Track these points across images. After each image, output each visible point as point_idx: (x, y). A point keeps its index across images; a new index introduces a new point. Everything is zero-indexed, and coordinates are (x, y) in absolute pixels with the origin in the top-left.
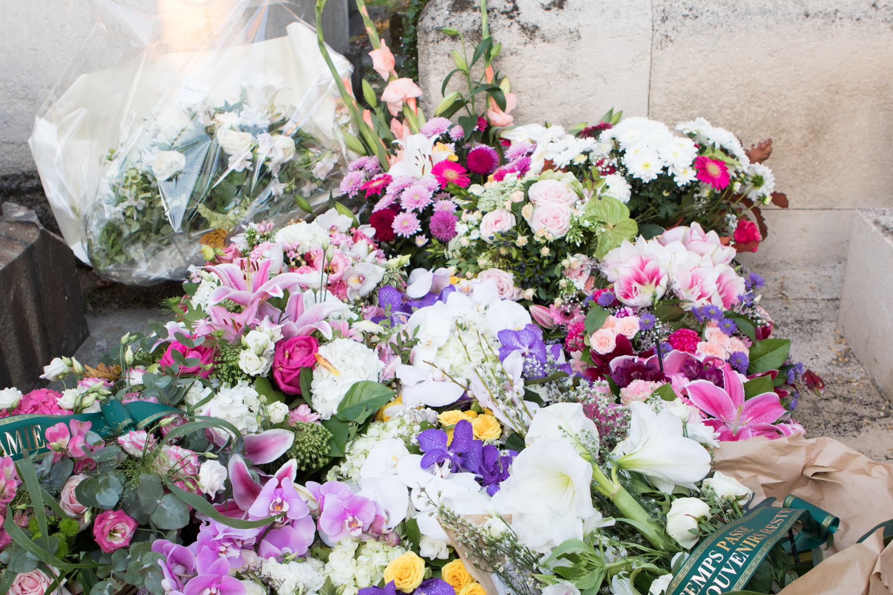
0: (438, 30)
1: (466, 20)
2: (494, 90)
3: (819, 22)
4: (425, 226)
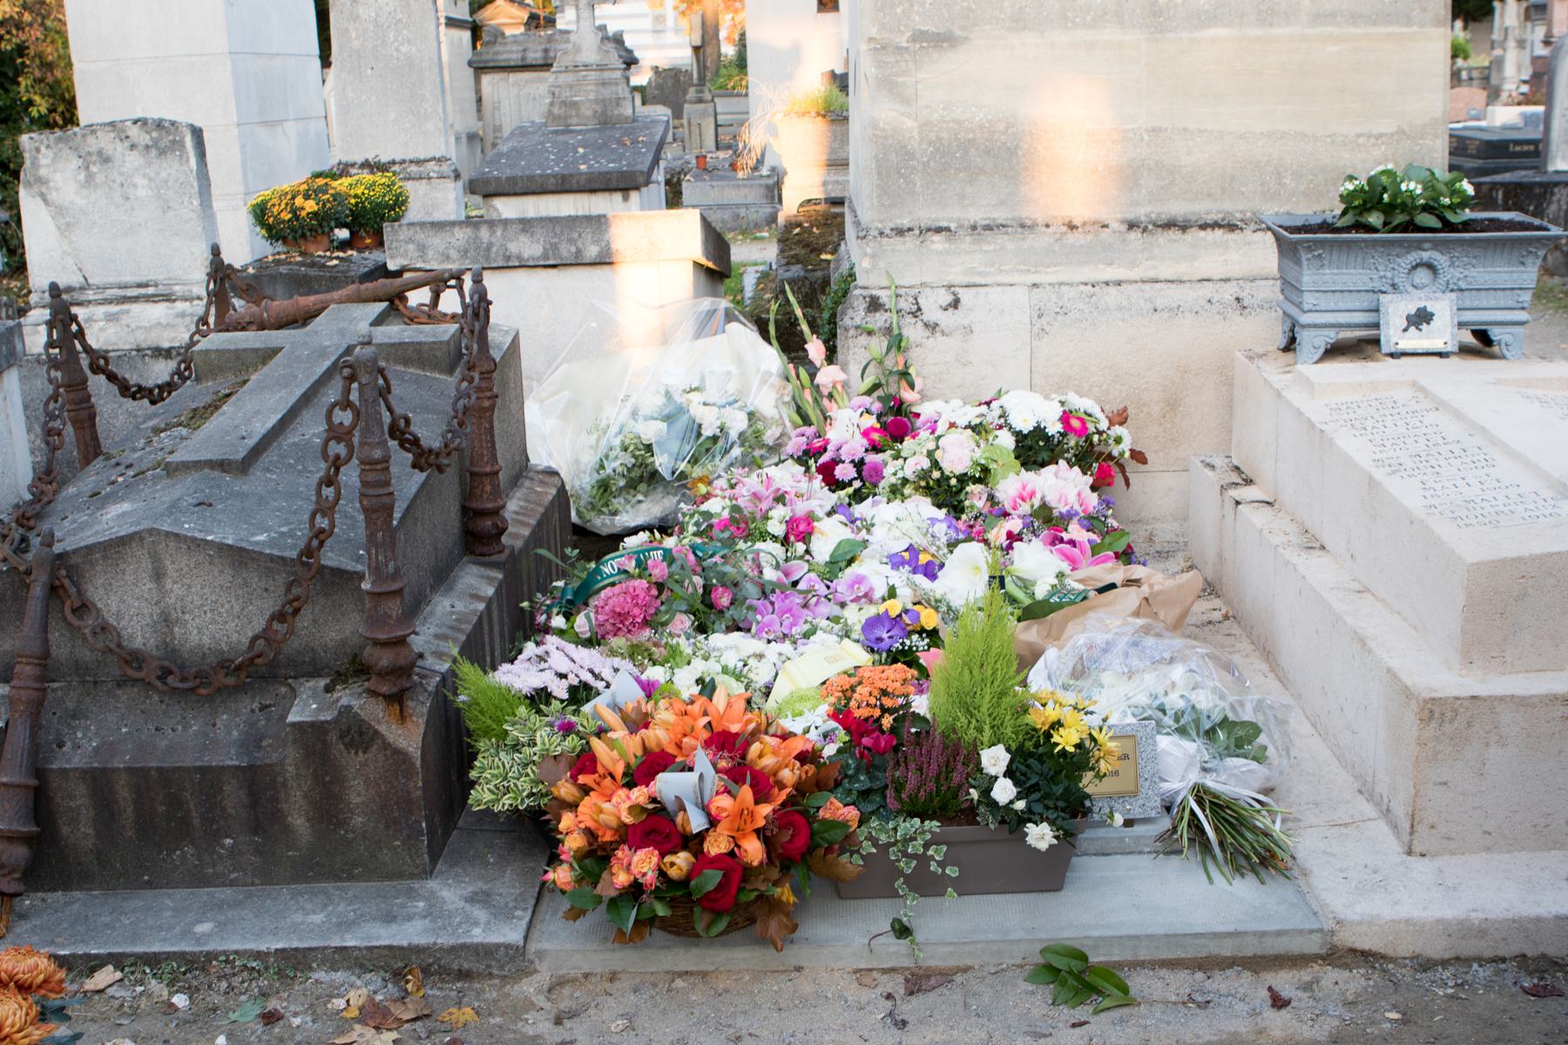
0: (857, 327)
1: (879, 319)
2: (904, 374)
3: (1166, 315)
4: (859, 472)
